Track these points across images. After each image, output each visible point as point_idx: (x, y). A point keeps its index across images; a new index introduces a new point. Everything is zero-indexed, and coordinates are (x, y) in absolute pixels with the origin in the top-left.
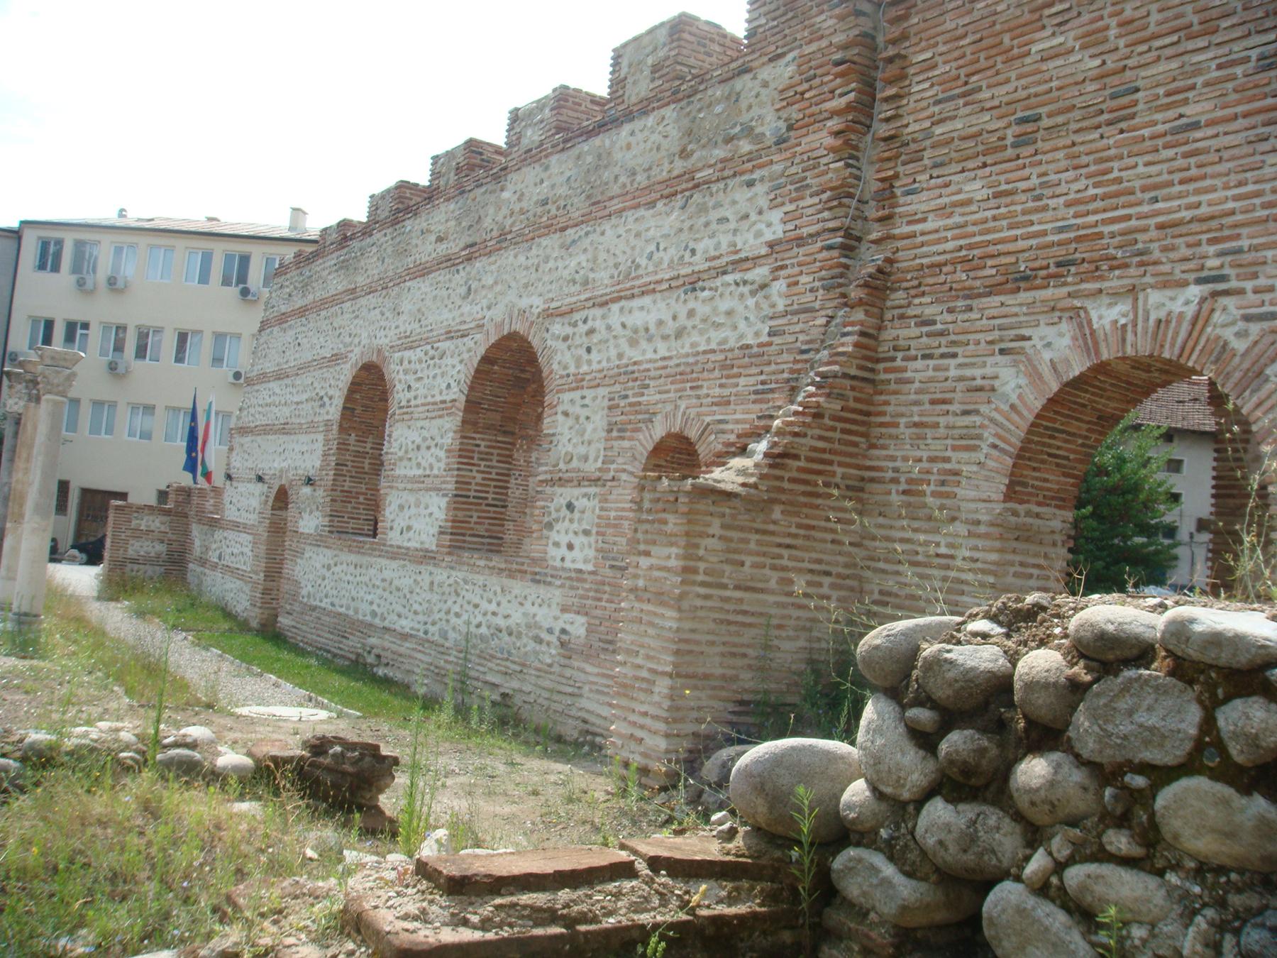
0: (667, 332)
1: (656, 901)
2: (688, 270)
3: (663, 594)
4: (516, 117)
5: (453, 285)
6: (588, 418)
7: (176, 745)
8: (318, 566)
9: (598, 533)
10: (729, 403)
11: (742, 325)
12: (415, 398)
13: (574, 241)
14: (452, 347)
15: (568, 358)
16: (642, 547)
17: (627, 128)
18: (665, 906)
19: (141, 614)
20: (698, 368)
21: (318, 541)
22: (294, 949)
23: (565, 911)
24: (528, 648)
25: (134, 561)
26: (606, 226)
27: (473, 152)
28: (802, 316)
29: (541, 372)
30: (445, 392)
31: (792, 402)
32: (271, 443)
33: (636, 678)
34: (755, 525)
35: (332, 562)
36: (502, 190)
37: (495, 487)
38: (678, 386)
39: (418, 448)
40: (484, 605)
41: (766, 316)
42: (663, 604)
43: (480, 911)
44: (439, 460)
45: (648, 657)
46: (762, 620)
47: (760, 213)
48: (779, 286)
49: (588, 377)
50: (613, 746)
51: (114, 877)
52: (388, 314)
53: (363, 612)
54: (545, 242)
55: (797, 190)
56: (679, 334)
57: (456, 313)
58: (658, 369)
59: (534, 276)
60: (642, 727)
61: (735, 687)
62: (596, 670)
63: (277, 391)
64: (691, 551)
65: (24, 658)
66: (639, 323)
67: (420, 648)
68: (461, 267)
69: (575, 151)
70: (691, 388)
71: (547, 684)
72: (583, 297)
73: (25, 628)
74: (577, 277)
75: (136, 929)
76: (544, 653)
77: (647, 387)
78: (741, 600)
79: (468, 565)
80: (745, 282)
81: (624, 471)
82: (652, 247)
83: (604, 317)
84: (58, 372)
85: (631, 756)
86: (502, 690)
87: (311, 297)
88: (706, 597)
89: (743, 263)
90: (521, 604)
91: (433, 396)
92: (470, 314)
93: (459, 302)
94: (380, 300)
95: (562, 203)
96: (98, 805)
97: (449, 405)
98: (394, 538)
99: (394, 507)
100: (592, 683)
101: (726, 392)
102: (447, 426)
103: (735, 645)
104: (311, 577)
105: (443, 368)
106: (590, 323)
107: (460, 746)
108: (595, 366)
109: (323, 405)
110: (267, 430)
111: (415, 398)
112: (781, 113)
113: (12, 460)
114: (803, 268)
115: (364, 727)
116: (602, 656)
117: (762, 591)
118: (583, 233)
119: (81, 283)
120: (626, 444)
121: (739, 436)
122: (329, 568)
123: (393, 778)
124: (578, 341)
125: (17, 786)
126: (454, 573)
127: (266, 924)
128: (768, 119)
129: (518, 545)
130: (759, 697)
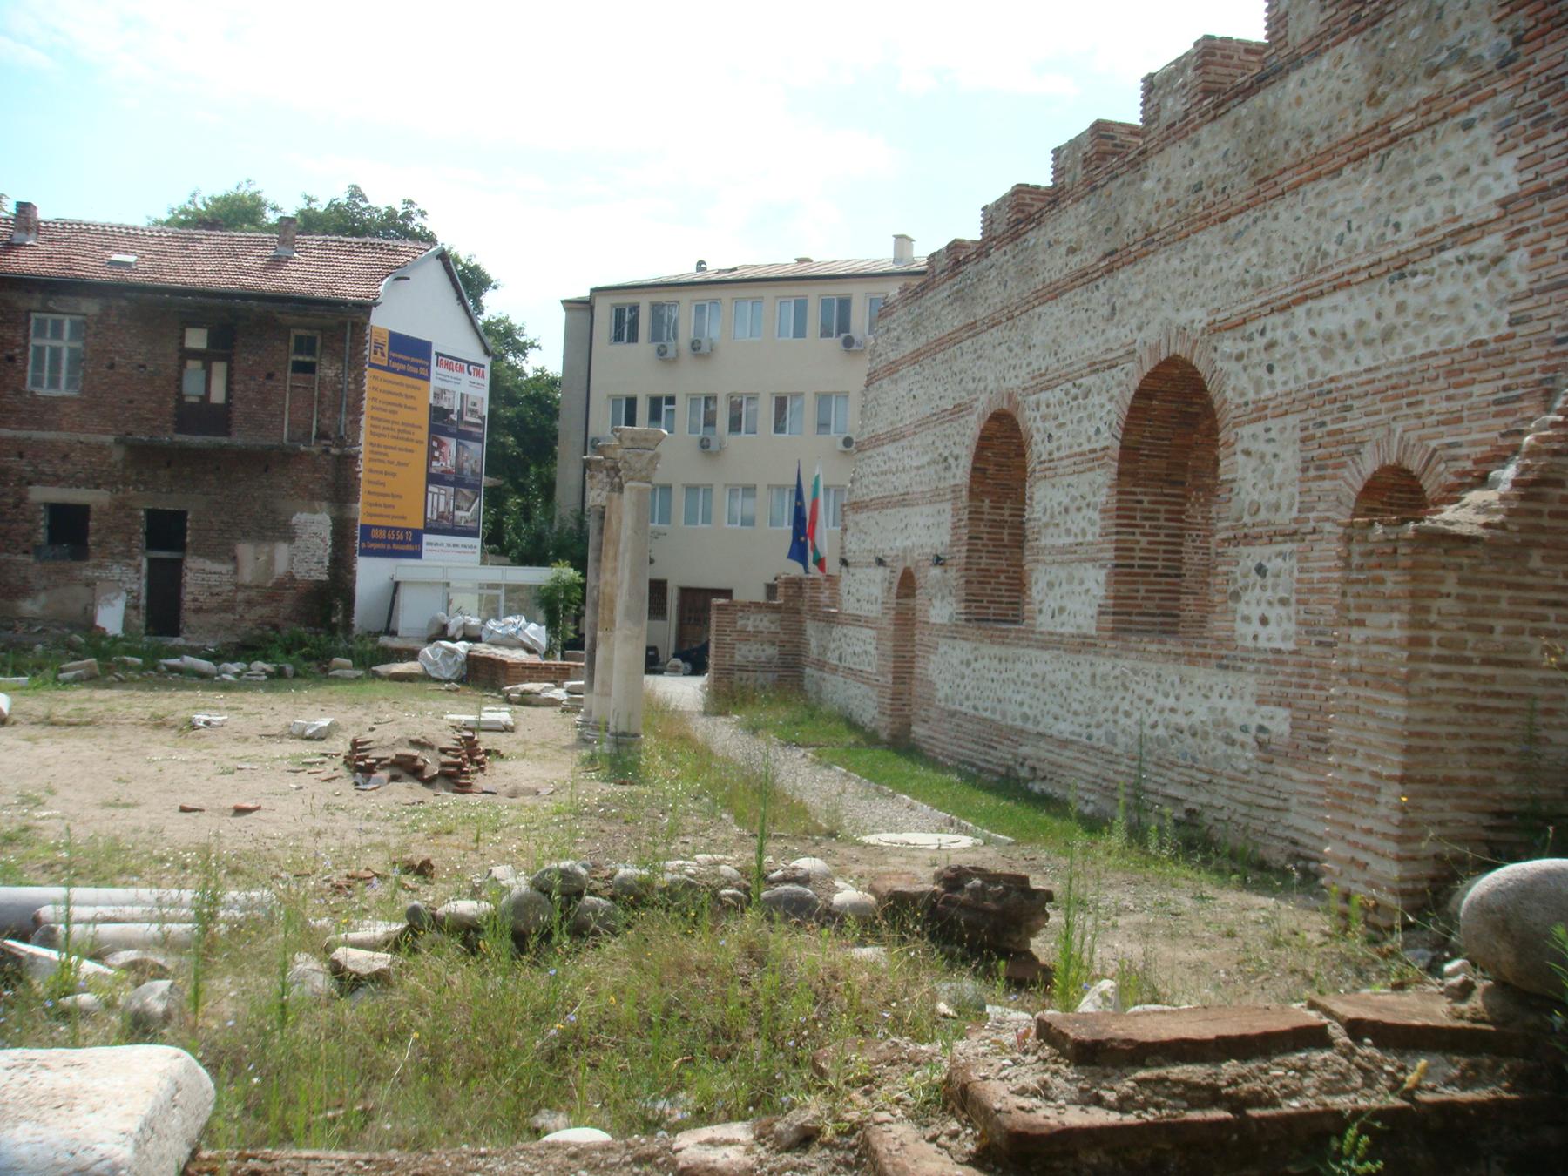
0: (1371, 335)
1: (1357, 1080)
2: (1392, 252)
3: (1384, 674)
4: (1151, 85)
5: (1093, 305)
6: (1275, 456)
7: (784, 880)
8: (955, 662)
9: (1298, 602)
10: (1460, 420)
11: (1471, 316)
12: (1058, 449)
13: (1240, 233)
14: (1098, 382)
15: (1244, 381)
16: (1353, 615)
17: (1294, 78)
18: (1370, 1087)
19: (754, 730)
20: (1417, 377)
21: (953, 633)
22: (886, 1127)
23: (1231, 1090)
24: (1218, 752)
25: (743, 668)
26: (1279, 207)
27: (1102, 136)
28: (1554, 294)
29: (1211, 402)
30: (1094, 438)
31: (1548, 411)
32: (891, 518)
33: (1355, 785)
34: (1507, 578)
35: (971, 657)
36: (1143, 179)
37: (1165, 552)
38: (1391, 404)
39: (1067, 510)
40: (1160, 700)
41: (1504, 299)
42: (1385, 687)
43: (1117, 1086)
44: (1093, 524)
45: (1369, 757)
46: (1523, 704)
47: (1485, 162)
48: (1520, 257)
49: (1272, 404)
50: (1335, 878)
51: (715, 1033)
52: (1017, 350)
53: (1012, 715)
54: (1202, 237)
55: (1534, 124)
56: (1387, 336)
57: (1100, 339)
58: (1362, 384)
59: (1192, 282)
60: (1365, 848)
61: (1489, 794)
62: (1306, 777)
63: (894, 455)
64: (1418, 617)
65: (623, 783)
66: (1333, 327)
67: (1083, 756)
68: (1100, 282)
69: (1231, 117)
70: (1409, 405)
71: (1243, 795)
72: (1257, 302)
73: (624, 749)
74: (1247, 277)
75: (741, 1094)
76: (1238, 757)
77: (1349, 409)
78: (1492, 679)
79: (1137, 651)
80: (1471, 258)
81: (1327, 519)
82: (1342, 228)
83: (1286, 325)
84: (639, 455)
85: (1353, 887)
86: (1187, 806)
87: (923, 339)
88: (1443, 676)
89: (1463, 233)
90: (1206, 697)
91: (1080, 445)
92: (1117, 338)
93: (1101, 326)
94: (1006, 333)
95: (1220, 186)
96: (697, 951)
97: (1100, 454)
98: (1044, 623)
99: (1042, 584)
100: (1301, 793)
101: (1456, 405)
102: (1100, 480)
103: (1487, 738)
104: (948, 676)
105: (1090, 409)
106: (1269, 335)
107: (1135, 877)
108: (1280, 389)
109: (948, 468)
110: (884, 503)
111: (1058, 449)
112: (1502, 25)
113: (598, 560)
114: (1552, 229)
115: (1016, 855)
116: (1313, 759)
117: (1521, 665)
118: (1250, 221)
119: (662, 352)
120: (1327, 485)
121: (1476, 462)
122: (968, 664)
123: (1047, 916)
124: (1255, 359)
125: (608, 927)
126: (1120, 662)
127: (856, 1094)
128: (1485, 35)
129: (1202, 623)
130: (1523, 807)
